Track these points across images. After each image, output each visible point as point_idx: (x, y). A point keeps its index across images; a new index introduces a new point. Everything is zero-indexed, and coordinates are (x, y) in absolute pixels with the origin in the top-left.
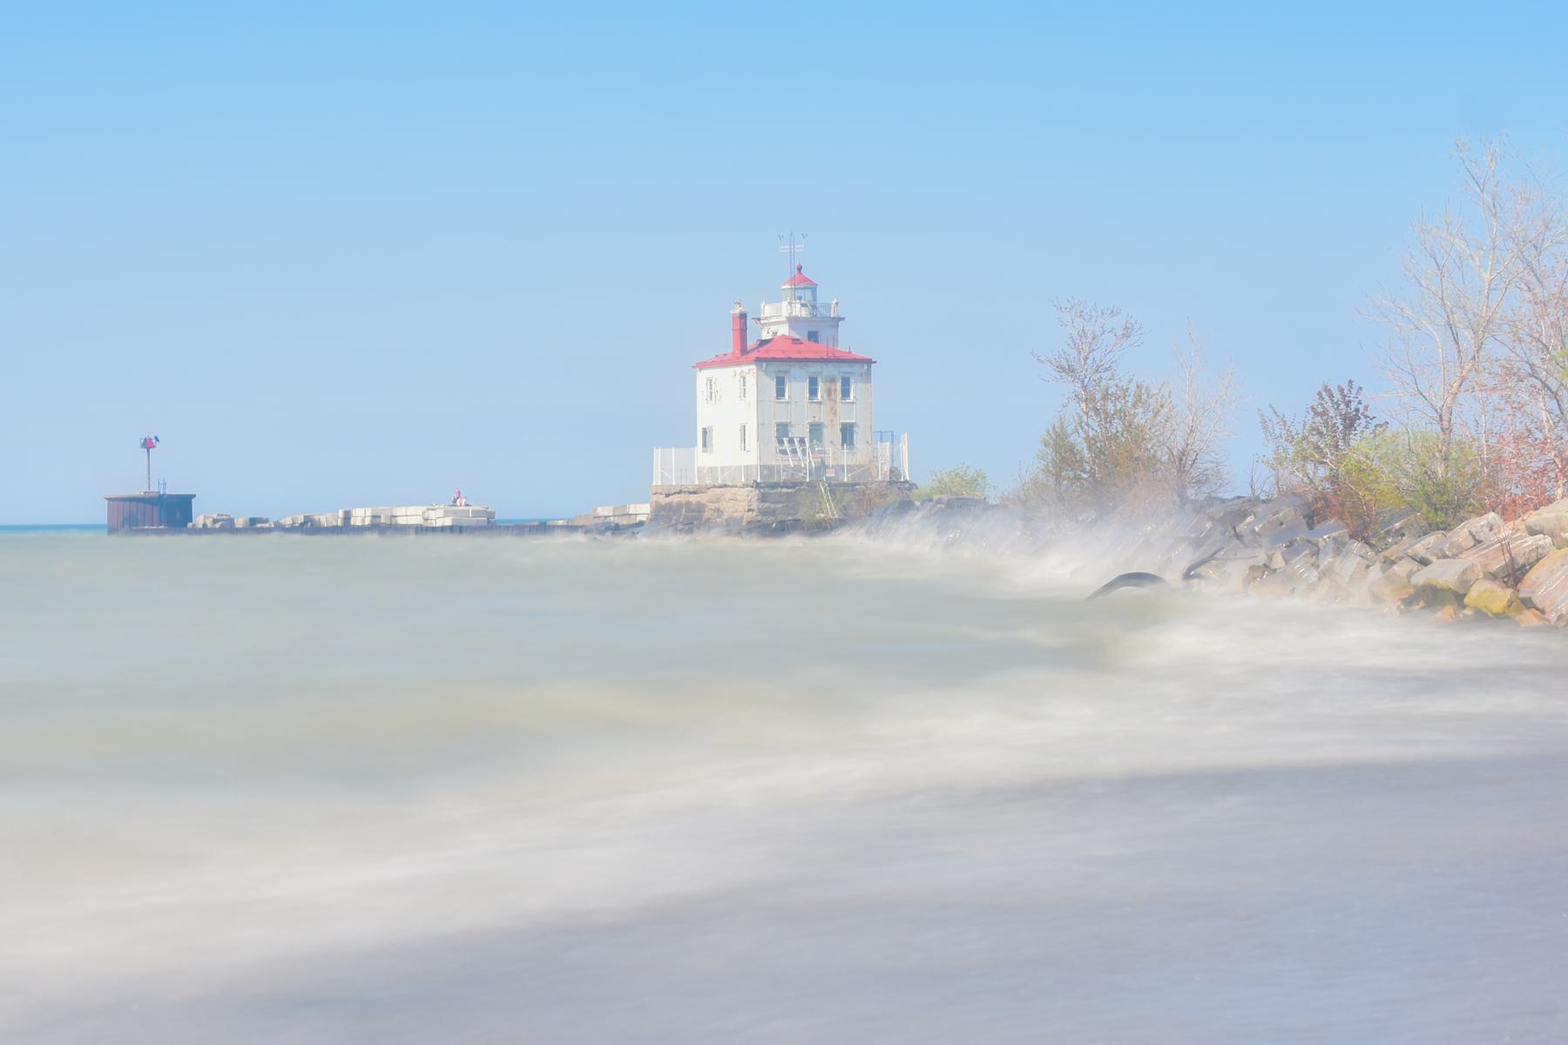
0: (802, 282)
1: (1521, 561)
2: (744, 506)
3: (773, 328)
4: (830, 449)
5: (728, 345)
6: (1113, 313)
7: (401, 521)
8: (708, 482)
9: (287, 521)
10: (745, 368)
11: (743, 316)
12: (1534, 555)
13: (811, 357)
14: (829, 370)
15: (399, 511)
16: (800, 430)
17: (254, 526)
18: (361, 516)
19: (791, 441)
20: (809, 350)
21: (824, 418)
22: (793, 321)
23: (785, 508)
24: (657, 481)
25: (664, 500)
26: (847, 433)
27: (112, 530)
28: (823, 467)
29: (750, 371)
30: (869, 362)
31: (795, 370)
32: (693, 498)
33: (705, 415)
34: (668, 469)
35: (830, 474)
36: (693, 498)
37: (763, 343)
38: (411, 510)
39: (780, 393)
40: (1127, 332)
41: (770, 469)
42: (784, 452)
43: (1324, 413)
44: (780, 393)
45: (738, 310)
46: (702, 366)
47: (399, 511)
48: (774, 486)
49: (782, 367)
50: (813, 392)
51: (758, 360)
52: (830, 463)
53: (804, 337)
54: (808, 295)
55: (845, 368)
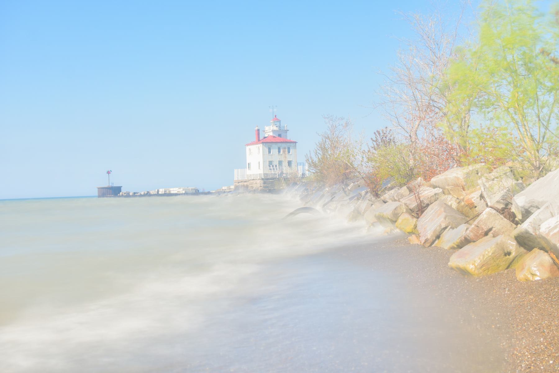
0: (276, 120)
1: (426, 202)
2: (259, 185)
3: (268, 134)
4: (284, 168)
5: (255, 139)
6: (342, 119)
7: (172, 192)
8: (250, 179)
9: (142, 193)
10: (259, 145)
11: (258, 130)
12: (433, 199)
13: (280, 142)
14: (284, 145)
15: (171, 189)
16: (276, 163)
17: (148, 194)
18: (161, 191)
19: (273, 166)
20: (278, 139)
21: (283, 159)
22: (274, 131)
23: (270, 184)
24: (236, 179)
25: (238, 184)
26: (290, 163)
27: (99, 196)
28: (282, 173)
29: (261, 146)
30: (296, 142)
31: (274, 145)
32: (245, 184)
33: (249, 159)
34: (238, 175)
35: (284, 175)
36: (245, 184)
37: (265, 138)
38: (175, 189)
39: (270, 152)
40: (347, 124)
41: (267, 174)
42: (271, 169)
43: (376, 141)
44: (270, 152)
45: (257, 128)
46: (248, 145)
47: (171, 189)
48: (268, 179)
49: (270, 144)
50: (279, 152)
51: (263, 143)
52: (285, 172)
53: (277, 136)
54: (278, 124)
55: (288, 144)
